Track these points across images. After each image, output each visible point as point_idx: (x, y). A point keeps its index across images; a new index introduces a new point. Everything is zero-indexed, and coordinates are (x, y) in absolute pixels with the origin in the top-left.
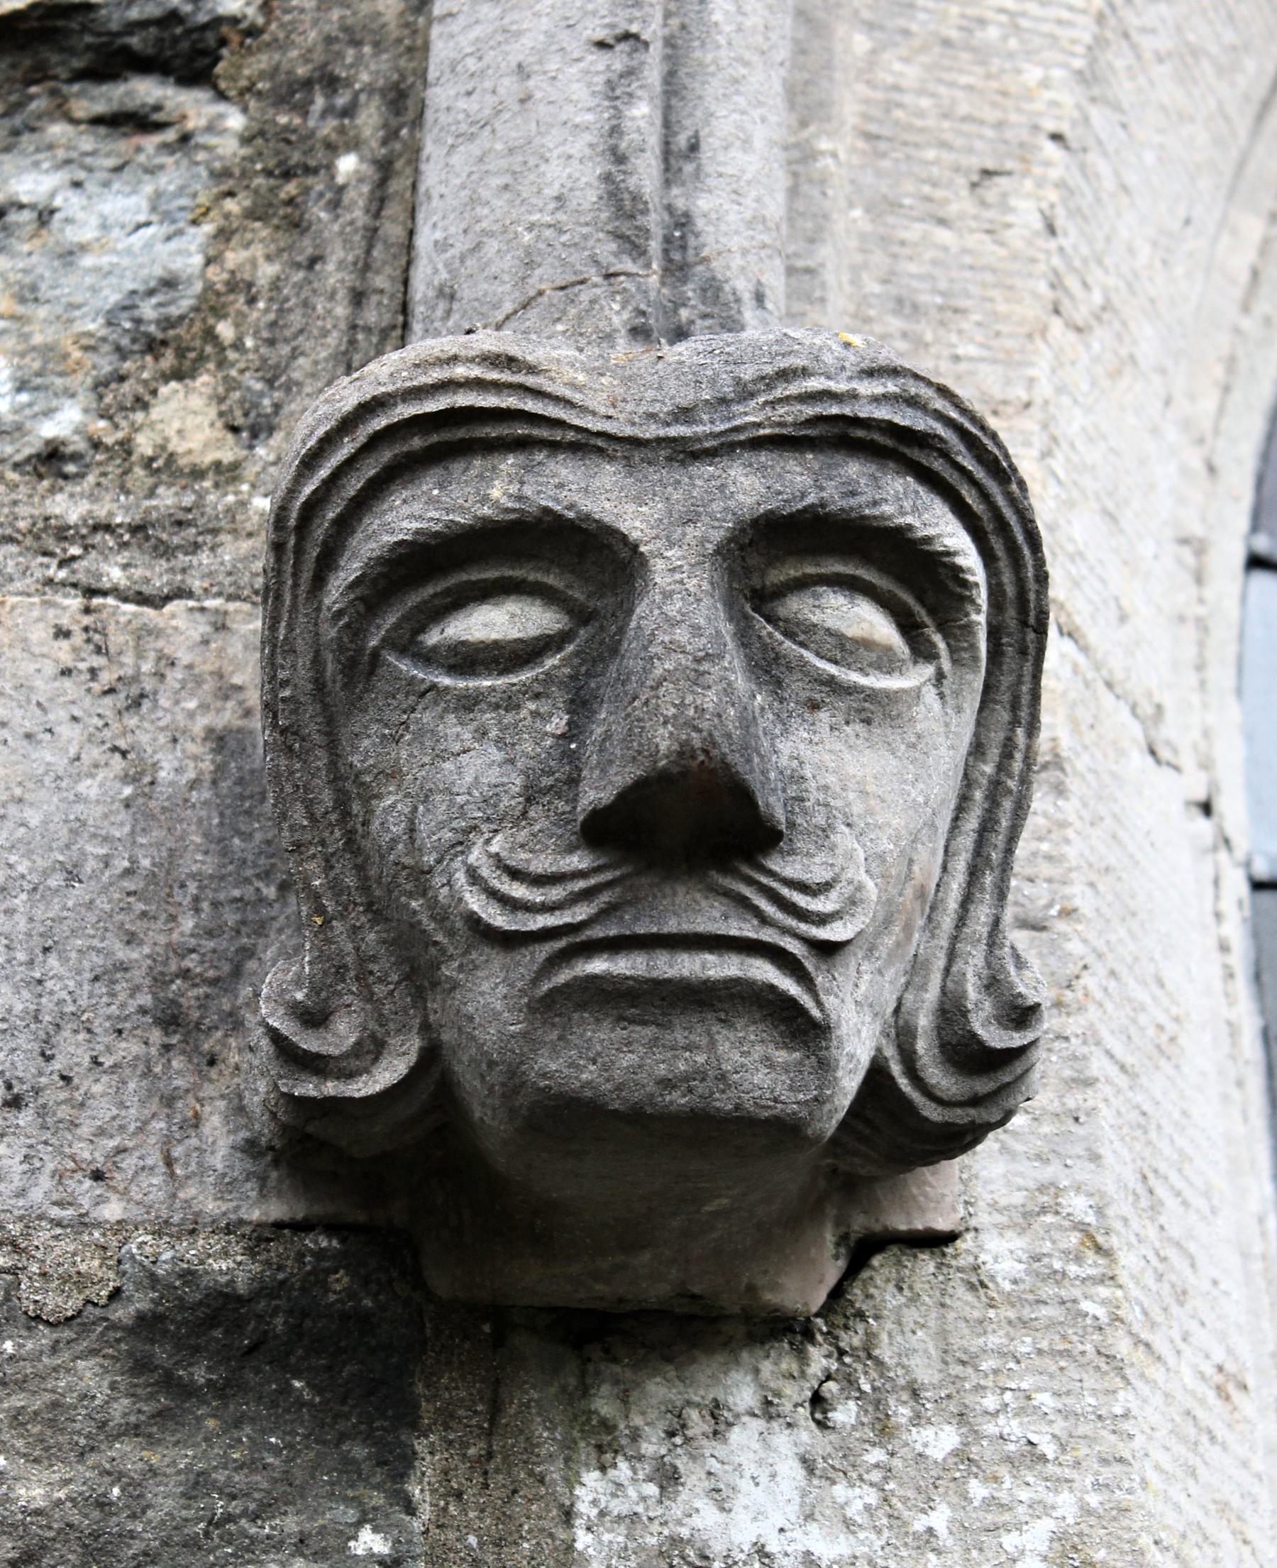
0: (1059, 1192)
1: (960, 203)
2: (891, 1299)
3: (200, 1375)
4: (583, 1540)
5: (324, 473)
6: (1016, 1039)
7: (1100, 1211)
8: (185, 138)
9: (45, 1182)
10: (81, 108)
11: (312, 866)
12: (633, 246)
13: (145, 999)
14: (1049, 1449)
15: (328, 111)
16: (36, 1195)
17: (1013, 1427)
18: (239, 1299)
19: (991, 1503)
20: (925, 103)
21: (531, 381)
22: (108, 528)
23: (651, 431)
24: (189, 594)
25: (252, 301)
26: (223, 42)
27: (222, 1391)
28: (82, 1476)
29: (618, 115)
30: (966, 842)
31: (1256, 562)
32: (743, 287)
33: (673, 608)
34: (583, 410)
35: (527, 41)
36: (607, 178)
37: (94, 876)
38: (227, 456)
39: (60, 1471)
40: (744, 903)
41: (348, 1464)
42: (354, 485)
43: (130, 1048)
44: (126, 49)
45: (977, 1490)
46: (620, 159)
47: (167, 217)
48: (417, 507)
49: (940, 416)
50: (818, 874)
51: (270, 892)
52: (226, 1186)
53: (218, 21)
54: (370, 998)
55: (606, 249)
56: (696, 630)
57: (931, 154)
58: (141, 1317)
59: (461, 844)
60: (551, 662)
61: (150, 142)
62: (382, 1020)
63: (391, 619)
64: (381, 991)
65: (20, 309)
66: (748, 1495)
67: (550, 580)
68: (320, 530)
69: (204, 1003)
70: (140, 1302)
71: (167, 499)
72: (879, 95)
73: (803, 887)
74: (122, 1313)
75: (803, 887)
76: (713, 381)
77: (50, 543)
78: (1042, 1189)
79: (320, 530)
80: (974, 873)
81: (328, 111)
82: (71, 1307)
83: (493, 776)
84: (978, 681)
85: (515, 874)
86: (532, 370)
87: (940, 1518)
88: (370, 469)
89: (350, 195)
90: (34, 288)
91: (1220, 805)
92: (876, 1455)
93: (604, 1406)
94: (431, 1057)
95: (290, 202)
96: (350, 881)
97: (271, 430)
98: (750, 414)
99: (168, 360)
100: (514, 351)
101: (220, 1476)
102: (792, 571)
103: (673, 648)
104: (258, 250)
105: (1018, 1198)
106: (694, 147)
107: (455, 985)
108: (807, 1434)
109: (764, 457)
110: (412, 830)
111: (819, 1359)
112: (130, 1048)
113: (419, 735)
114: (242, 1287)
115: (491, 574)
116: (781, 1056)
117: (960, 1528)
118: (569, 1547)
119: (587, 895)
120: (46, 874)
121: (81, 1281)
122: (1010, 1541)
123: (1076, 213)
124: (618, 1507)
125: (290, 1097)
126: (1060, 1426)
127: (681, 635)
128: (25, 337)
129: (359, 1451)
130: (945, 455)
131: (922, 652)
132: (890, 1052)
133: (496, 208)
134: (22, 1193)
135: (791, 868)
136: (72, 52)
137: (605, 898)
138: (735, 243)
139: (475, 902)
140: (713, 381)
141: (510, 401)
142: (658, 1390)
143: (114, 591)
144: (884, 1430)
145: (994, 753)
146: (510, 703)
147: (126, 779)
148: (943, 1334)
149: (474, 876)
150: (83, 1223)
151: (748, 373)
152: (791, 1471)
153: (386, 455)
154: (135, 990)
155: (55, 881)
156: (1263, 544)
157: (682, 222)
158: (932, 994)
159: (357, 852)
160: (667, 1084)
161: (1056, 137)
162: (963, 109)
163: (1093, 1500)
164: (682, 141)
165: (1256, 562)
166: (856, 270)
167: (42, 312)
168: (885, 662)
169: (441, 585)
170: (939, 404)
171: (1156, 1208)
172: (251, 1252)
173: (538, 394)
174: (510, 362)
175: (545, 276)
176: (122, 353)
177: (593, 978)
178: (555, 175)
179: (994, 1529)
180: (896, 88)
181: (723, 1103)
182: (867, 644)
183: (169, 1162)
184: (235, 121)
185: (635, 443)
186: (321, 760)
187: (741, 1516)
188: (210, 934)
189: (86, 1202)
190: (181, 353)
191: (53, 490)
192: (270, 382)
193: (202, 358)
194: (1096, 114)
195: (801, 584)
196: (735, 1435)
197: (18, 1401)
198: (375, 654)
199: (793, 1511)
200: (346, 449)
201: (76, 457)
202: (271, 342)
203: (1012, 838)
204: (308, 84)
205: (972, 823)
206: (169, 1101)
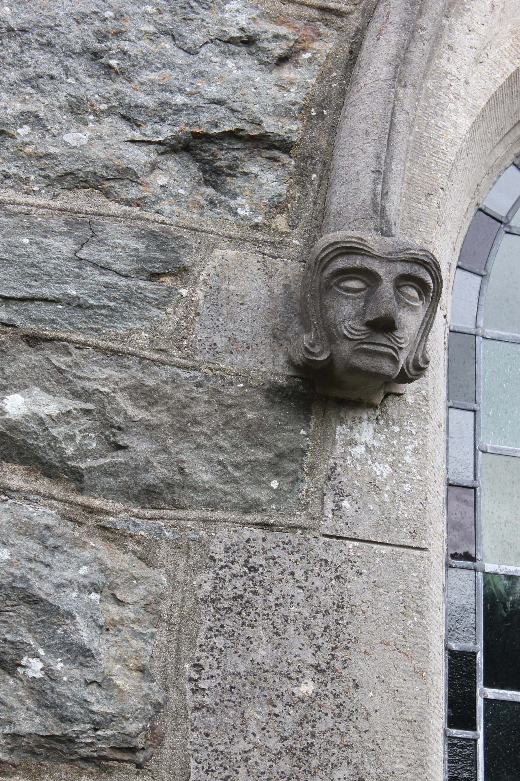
0: (421, 389)
1: (423, 200)
2: (391, 404)
3: (277, 400)
4: (337, 437)
5: (326, 252)
6: (425, 366)
7: (427, 394)
8: (283, 165)
9: (253, 363)
10: (264, 155)
11: (314, 319)
12: (376, 213)
13: (271, 332)
14: (414, 433)
15: (311, 164)
16: (251, 364)
17: (409, 429)
18: (284, 388)
19: (404, 441)
20: (419, 178)
21: (365, 243)
22: (267, 242)
23: (384, 256)
24: (281, 258)
25: (294, 201)
26: (292, 146)
27: (280, 403)
28: (258, 414)
29: (375, 186)
30: (422, 331)
31: (458, 267)
32: (393, 222)
33: (387, 289)
34: (373, 250)
35: (359, 167)
36: (372, 199)
37: (263, 308)
38: (288, 231)
39: (254, 413)
40: (389, 339)
41: (299, 418)
42: (332, 256)
43: (267, 341)
44: (274, 145)
45: (402, 438)
46: (375, 195)
47: (280, 181)
48: (343, 262)
49: (431, 259)
50: (401, 336)
51: (293, 316)
52: (283, 368)
53: (292, 142)
54: (322, 343)
55: (371, 213)
56: (390, 294)
57: (419, 189)
58: (268, 388)
59: (344, 322)
60: (362, 293)
61: (277, 164)
62: (324, 348)
63: (335, 280)
64: (324, 342)
65: (251, 195)
66: (365, 433)
67: (364, 279)
68: (325, 262)
69: (280, 335)
70: (268, 386)
71: (277, 238)
72: (411, 175)
73: (399, 338)
74: (265, 387)
75: (399, 338)
76: (395, 248)
77: (256, 243)
78: (418, 388)
79: (325, 262)
80: (422, 337)
81: (311, 164)
82: (256, 385)
83: (350, 311)
84: (428, 305)
85: (353, 329)
86: (365, 241)
87: (395, 442)
88: (335, 254)
89: (314, 183)
90: (254, 191)
91: (447, 316)
92: (386, 430)
93: (342, 415)
94: (331, 355)
95: (303, 182)
96: (321, 323)
97: (297, 227)
98: (401, 255)
99: (278, 210)
100: (362, 237)
101: (280, 418)
102: (404, 283)
103: (386, 296)
104: (296, 190)
105: (414, 389)
106: (387, 193)
107: (338, 345)
108: (375, 425)
109: (402, 263)
110: (335, 317)
111: (378, 412)
112: (267, 341)
113: (338, 301)
114: (284, 386)
115: (354, 276)
116: (391, 365)
117: (398, 444)
118: (335, 438)
119: (364, 334)
120: (254, 307)
121: (258, 381)
122: (406, 447)
123: (443, 203)
124: (343, 432)
125: (307, 359)
126: (416, 429)
127: (387, 294)
128: (252, 201)
129: (301, 416)
130: (431, 266)
131: (421, 299)
132: (405, 365)
133: (350, 200)
134: (249, 364)
135: (397, 335)
136: (264, 144)
137: (367, 335)
138: (392, 213)
139: (345, 332)
140: (395, 248)
141: (361, 247)
142: (351, 414)
143: (267, 254)
144: (388, 426)
145: (429, 316)
146: (354, 299)
147: (269, 291)
148: (399, 411)
149: (345, 327)
150: (259, 371)
151: (401, 248)
152: (372, 430)
153: (338, 252)
154: (269, 330)
155: (256, 308)
156: (460, 263)
157: (384, 208)
158: (413, 357)
159: (322, 318)
160: (373, 367)
161: (442, 188)
162: (426, 180)
163: (421, 443)
164: (385, 191)
165: (458, 267)
166: (403, 210)
167: (256, 196)
168: (416, 301)
169: (345, 276)
170: (431, 257)
171: (434, 394)
172: (286, 380)
173: (366, 246)
174: (362, 239)
175: (359, 215)
176: (271, 207)
177: (364, 348)
178: (363, 196)
179: (404, 445)
180: (414, 174)
181: (381, 372)
182: (414, 297)
183: (273, 362)
184: (293, 163)
185: (381, 257)
186: (318, 301)
187: (363, 437)
188: (282, 322)
189: (259, 367)
190: (281, 209)
191: (256, 232)
192: (297, 217)
193: (284, 210)
194: (449, 184)
195: (405, 286)
196: (363, 423)
197: (248, 400)
198: (332, 286)
199: (371, 437)
200: (331, 249)
201: (261, 227)
202: (298, 210)
203: (429, 331)
204: (307, 157)
205: (423, 328)
206: (274, 351)
